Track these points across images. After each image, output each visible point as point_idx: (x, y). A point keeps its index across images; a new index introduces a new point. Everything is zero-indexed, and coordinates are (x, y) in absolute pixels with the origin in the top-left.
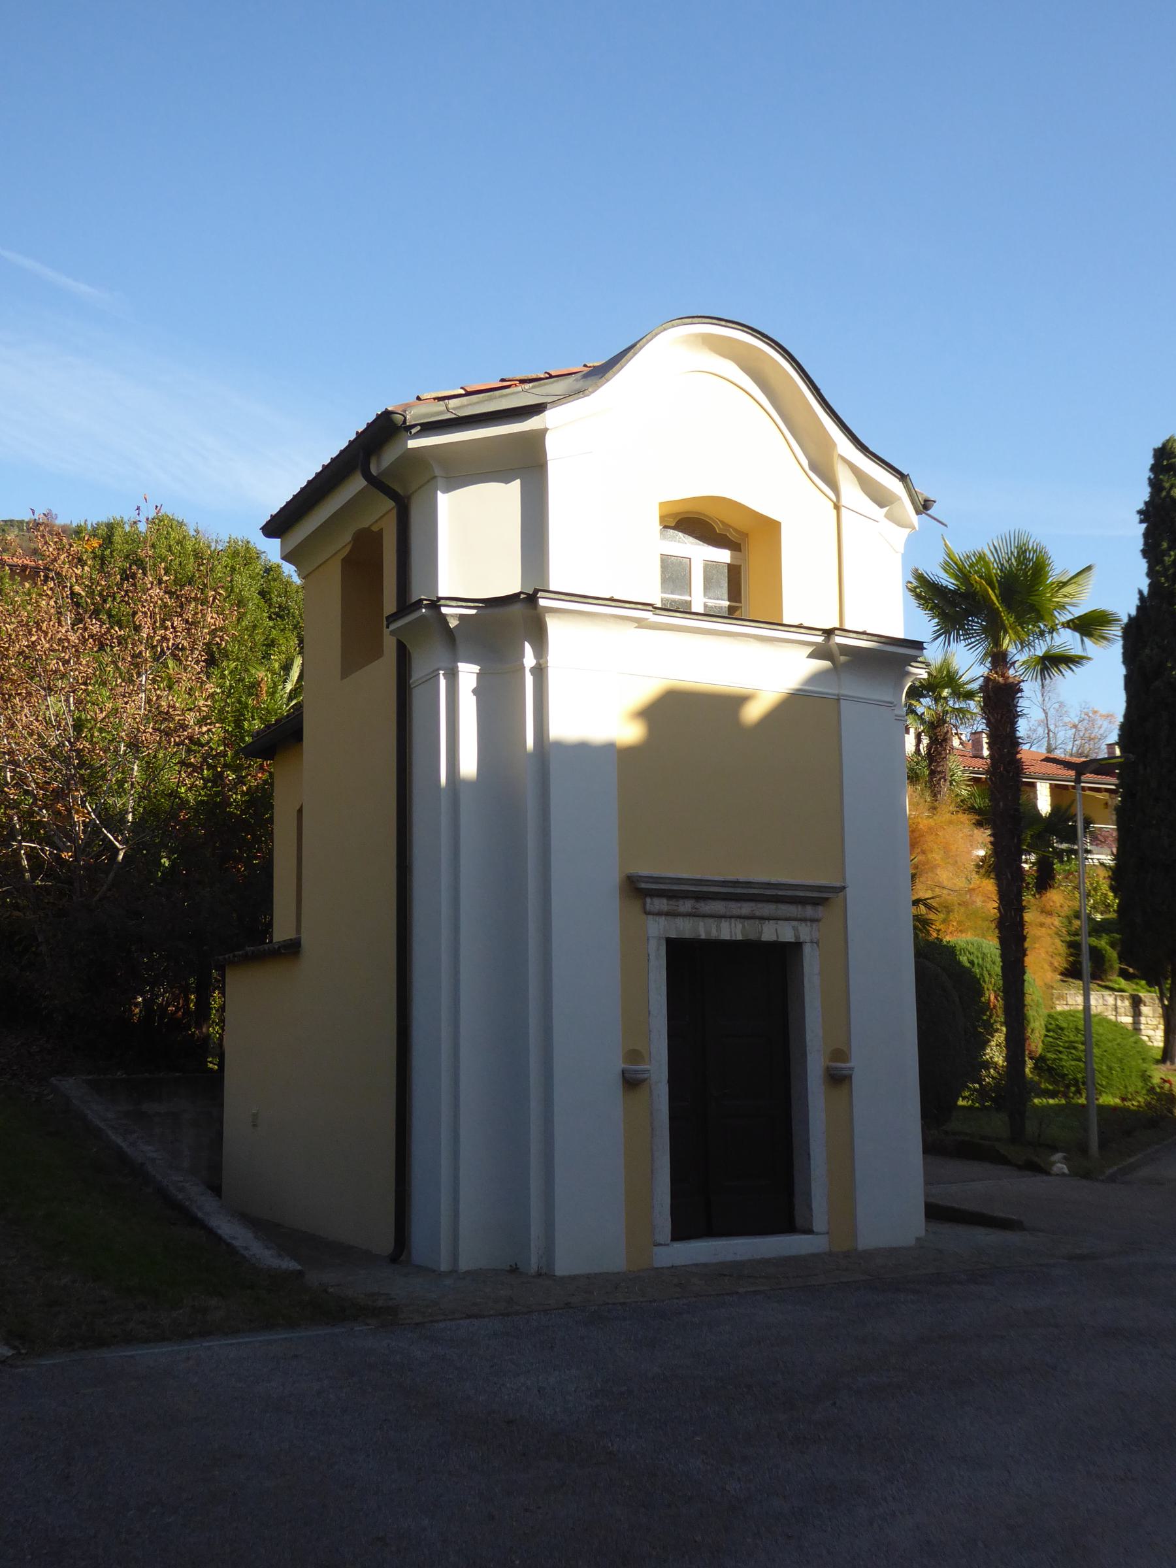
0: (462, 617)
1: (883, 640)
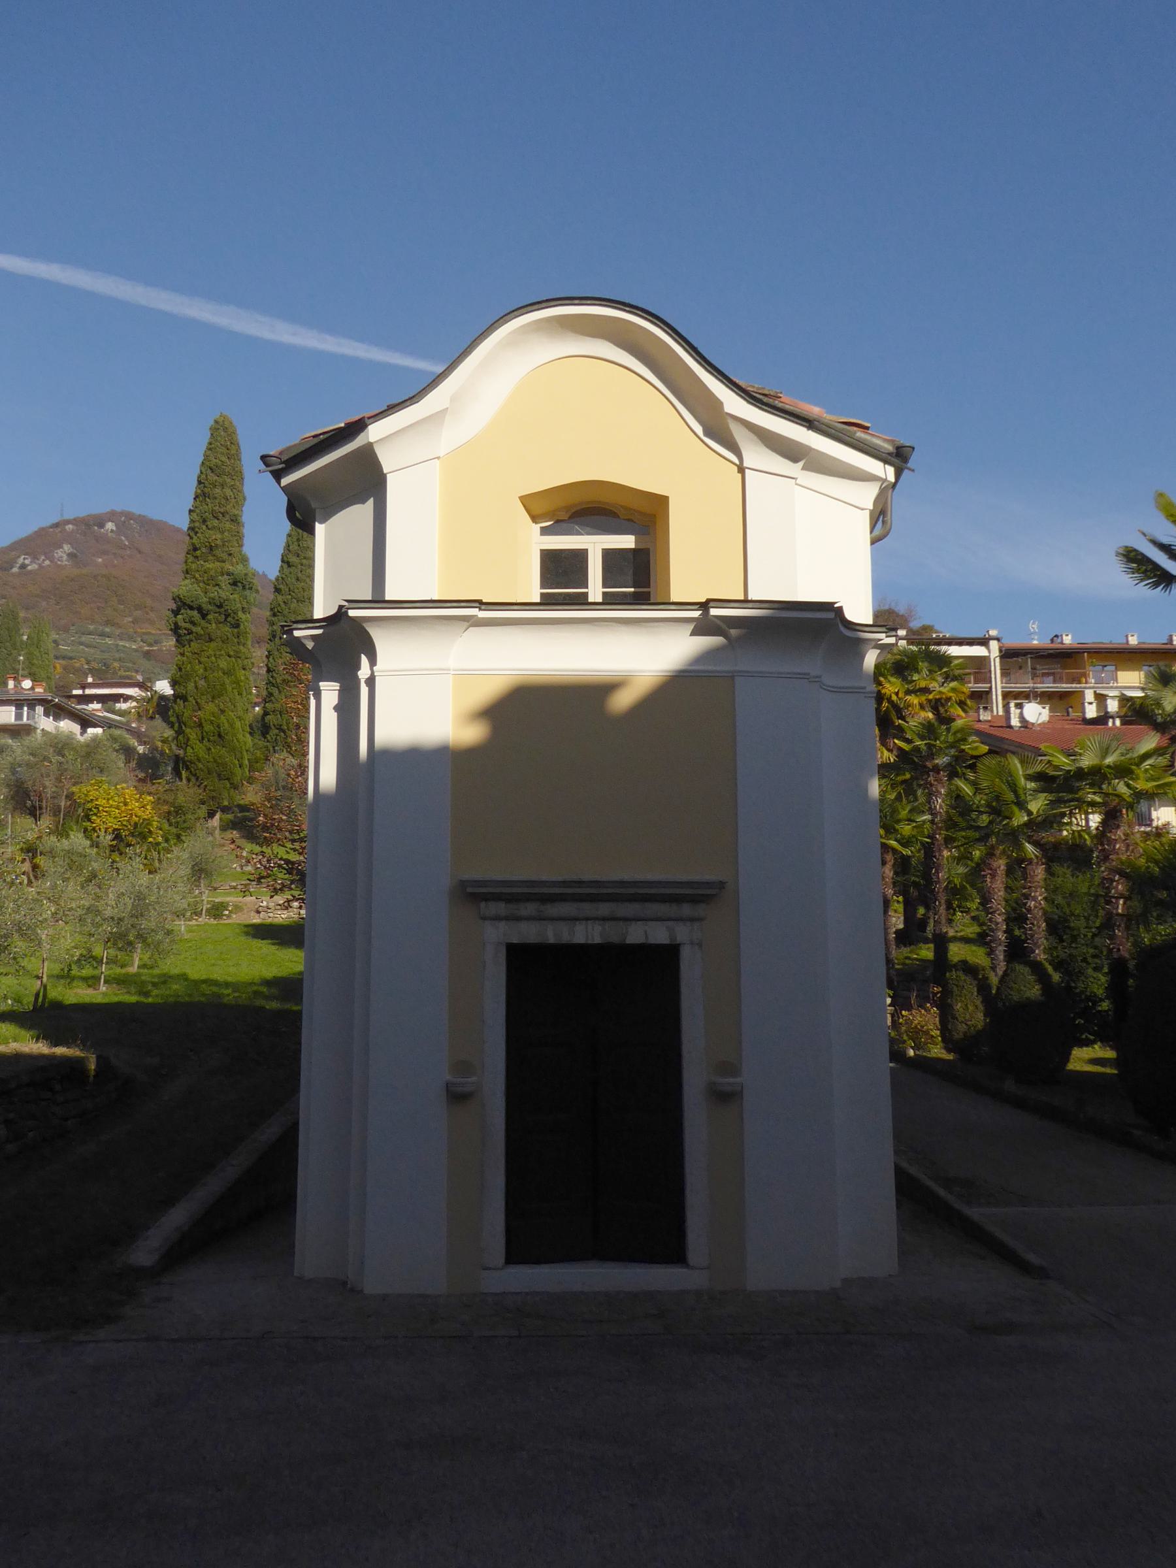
0: (313, 637)
1: (776, 606)
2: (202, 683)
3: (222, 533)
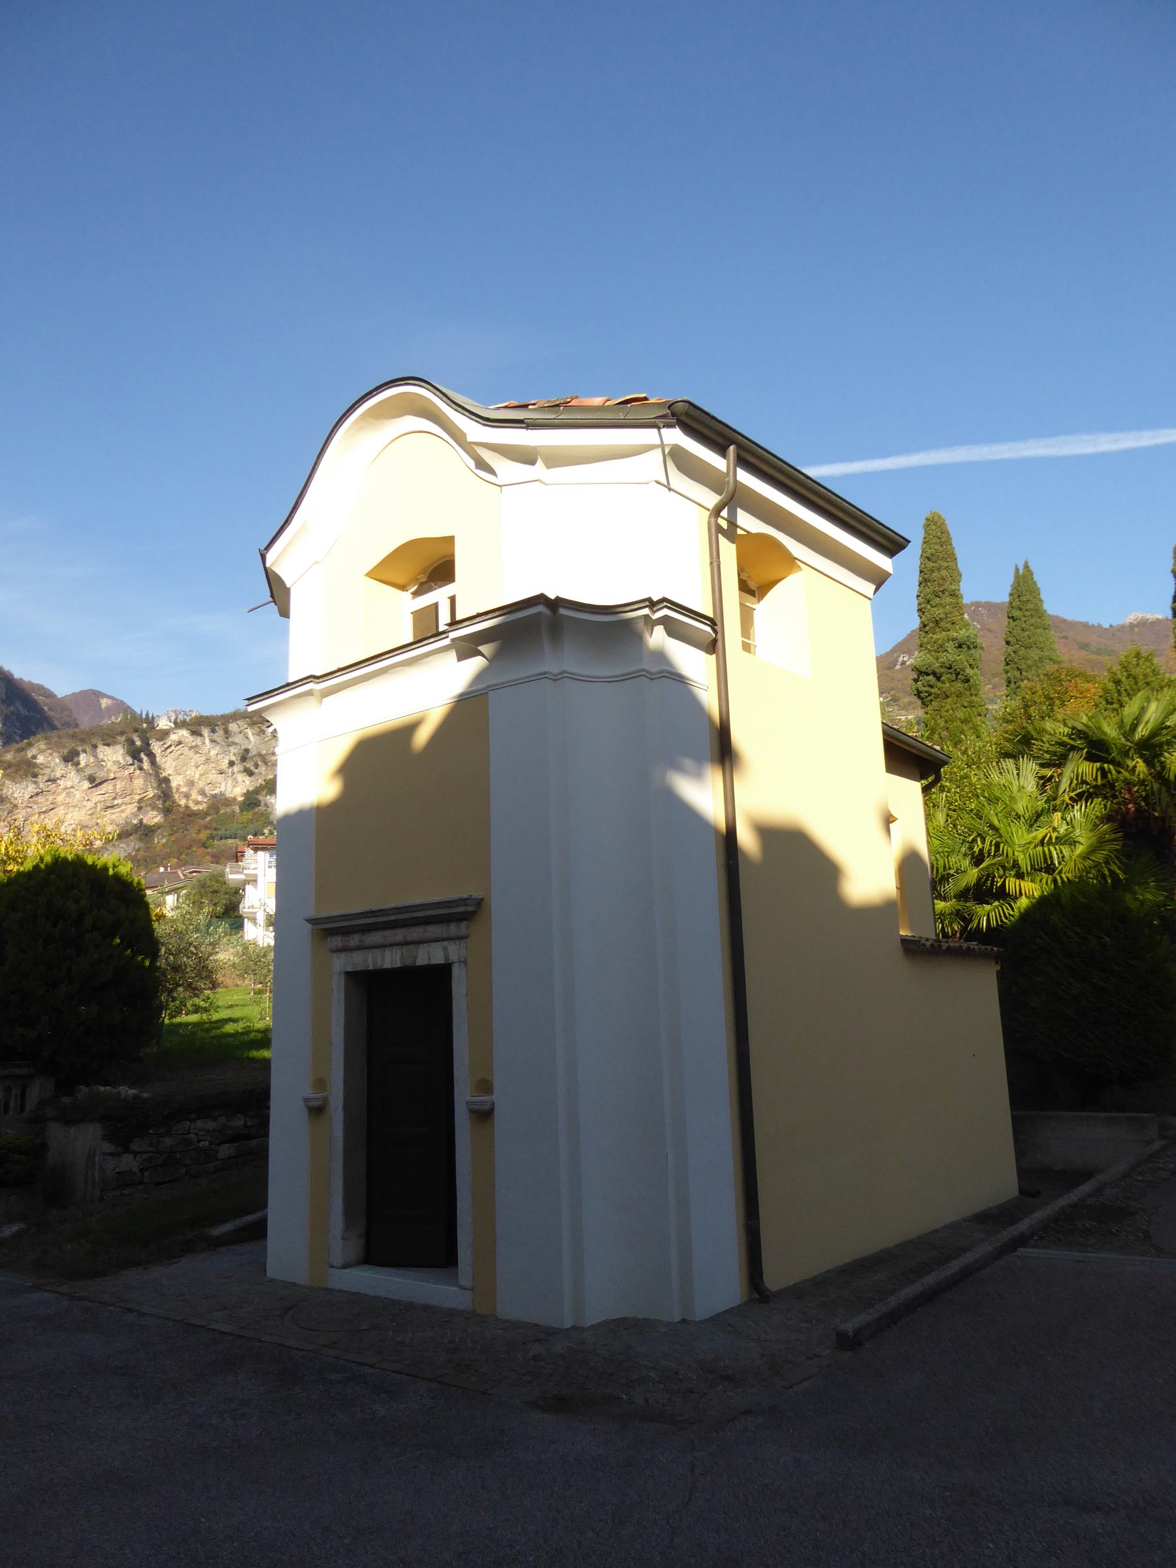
2: (944, 733)
3: (944, 607)
